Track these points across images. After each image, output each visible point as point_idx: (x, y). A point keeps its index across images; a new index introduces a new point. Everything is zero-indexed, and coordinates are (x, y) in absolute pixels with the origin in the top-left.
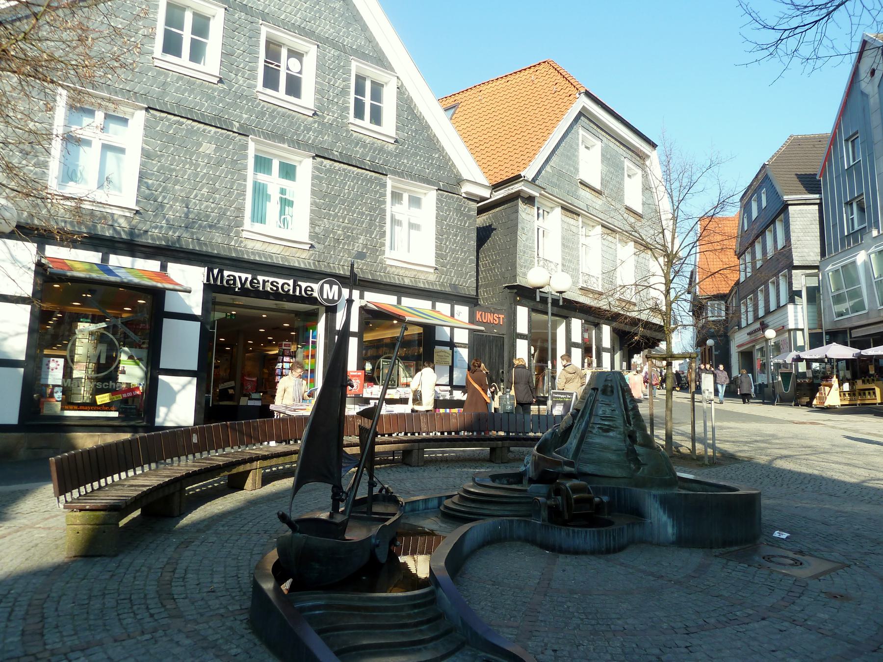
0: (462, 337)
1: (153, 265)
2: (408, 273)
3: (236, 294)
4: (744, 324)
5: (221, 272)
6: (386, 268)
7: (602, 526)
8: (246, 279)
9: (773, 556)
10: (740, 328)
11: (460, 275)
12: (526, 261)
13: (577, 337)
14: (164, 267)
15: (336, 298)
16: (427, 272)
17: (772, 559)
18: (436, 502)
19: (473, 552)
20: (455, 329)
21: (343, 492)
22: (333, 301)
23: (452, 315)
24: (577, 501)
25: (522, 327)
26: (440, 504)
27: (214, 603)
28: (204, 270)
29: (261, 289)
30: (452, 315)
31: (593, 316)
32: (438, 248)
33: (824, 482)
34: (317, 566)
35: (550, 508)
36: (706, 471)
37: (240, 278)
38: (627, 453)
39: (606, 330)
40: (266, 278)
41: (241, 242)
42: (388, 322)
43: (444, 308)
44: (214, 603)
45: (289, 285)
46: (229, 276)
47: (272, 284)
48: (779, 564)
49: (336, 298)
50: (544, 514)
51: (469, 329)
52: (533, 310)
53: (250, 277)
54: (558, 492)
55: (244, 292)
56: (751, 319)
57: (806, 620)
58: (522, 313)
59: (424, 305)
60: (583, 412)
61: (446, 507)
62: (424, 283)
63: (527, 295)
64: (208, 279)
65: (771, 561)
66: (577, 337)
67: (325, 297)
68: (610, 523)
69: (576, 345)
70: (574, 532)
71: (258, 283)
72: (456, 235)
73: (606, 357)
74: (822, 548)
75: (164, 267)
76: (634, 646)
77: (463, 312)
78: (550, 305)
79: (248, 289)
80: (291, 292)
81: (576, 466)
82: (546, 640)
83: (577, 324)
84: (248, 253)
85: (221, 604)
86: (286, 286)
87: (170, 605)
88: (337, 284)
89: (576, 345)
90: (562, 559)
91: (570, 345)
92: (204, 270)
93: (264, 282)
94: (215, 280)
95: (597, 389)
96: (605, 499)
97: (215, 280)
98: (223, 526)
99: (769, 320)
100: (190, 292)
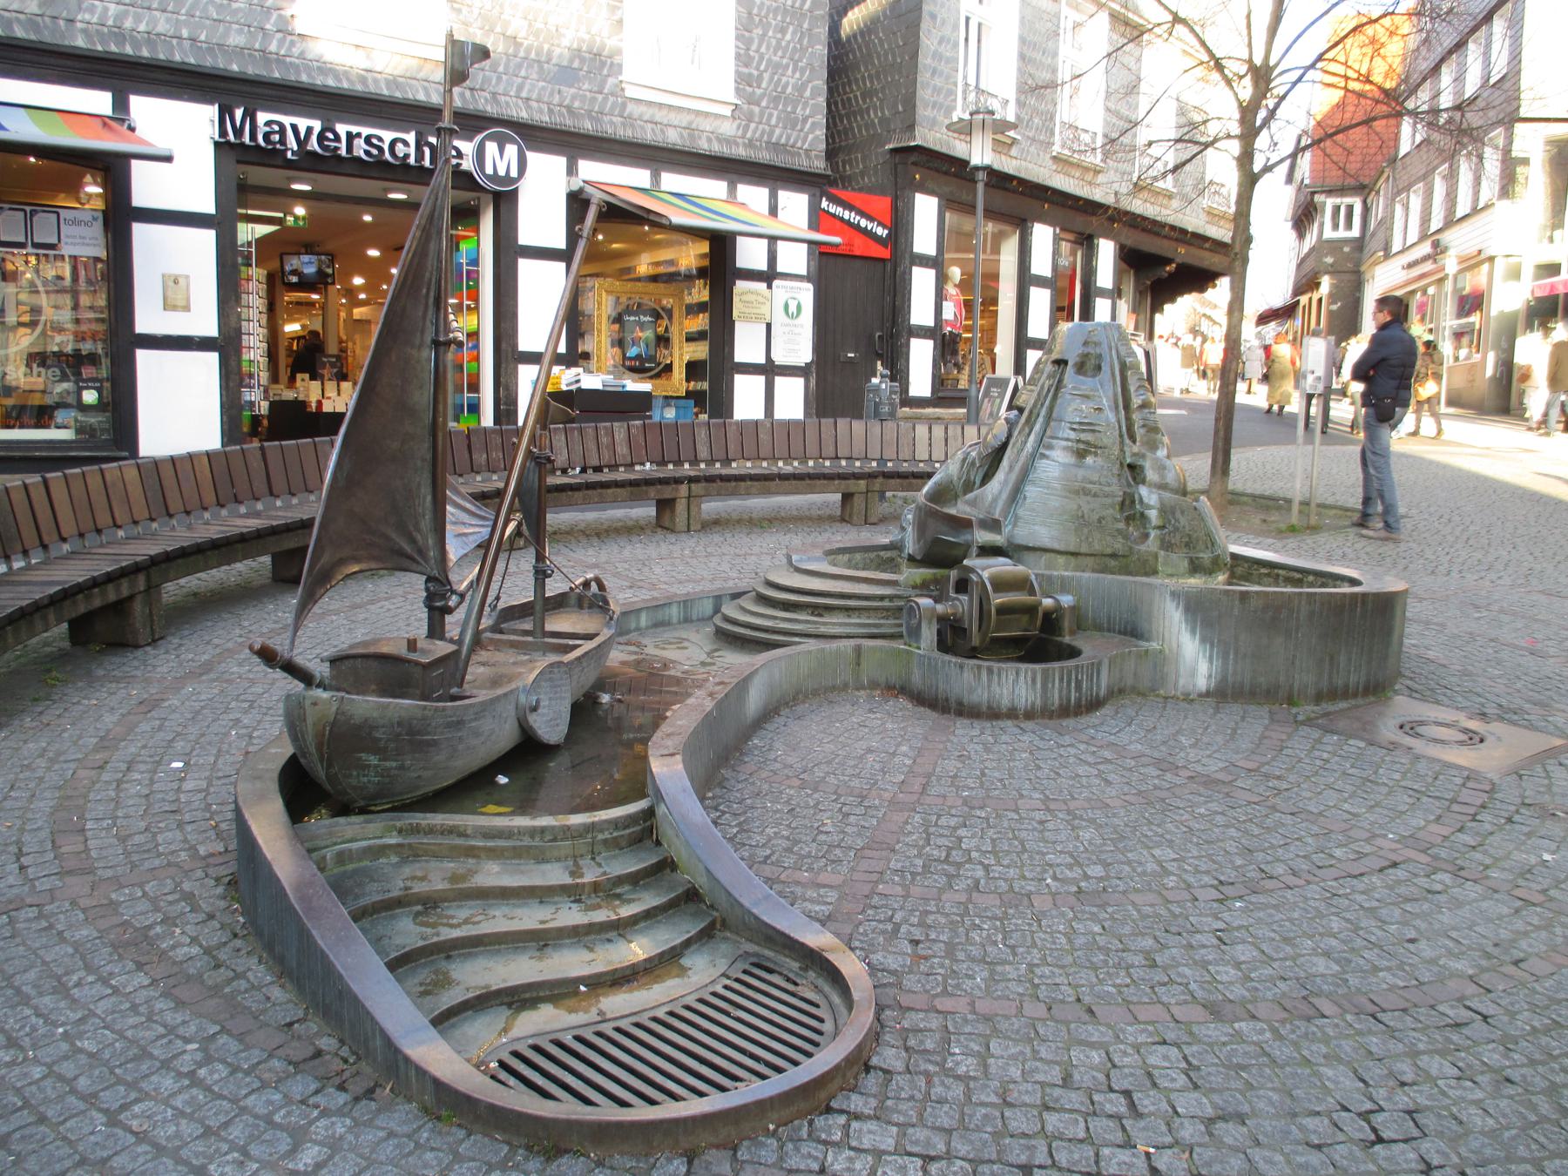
0: (794, 259)
1: (98, 101)
2: (674, 118)
3: (290, 165)
4: (1396, 247)
5: (250, 114)
6: (624, 105)
7: (1059, 658)
8: (309, 130)
9: (1422, 723)
10: (1387, 256)
11: (790, 122)
12: (938, 91)
13: (1041, 264)
14: (121, 105)
15: (514, 173)
16: (717, 116)
17: (1420, 730)
18: (708, 607)
19: (768, 714)
20: (779, 243)
21: (453, 592)
22: (508, 179)
23: (773, 211)
24: (1003, 610)
25: (924, 239)
26: (717, 610)
27: (169, 838)
28: (212, 111)
29: (343, 152)
30: (773, 211)
31: (1081, 218)
32: (743, 59)
33: (167, 473)
34: (373, 760)
35: (942, 619)
36: (1292, 542)
37: (295, 128)
38: (1122, 504)
39: (1106, 251)
40: (355, 129)
41: (293, 43)
42: (636, 229)
43: (754, 196)
44: (169, 838)
45: (406, 143)
46: (268, 123)
47: (368, 140)
48: (1436, 741)
49: (514, 173)
50: (929, 634)
51: (810, 242)
52: (949, 203)
53: (317, 125)
54: (962, 586)
55: (309, 162)
56: (1413, 236)
57: (1487, 867)
58: (926, 208)
59: (711, 188)
60: (1031, 412)
61: (727, 619)
62: (709, 140)
63: (948, 173)
64: (223, 133)
65: (1419, 735)
66: (1041, 264)
67: (489, 170)
68: (1074, 653)
69: (1041, 282)
70: (990, 671)
71: (337, 138)
72: (783, 31)
73: (1102, 308)
74: (1527, 706)
75: (121, 105)
76: (1097, 929)
77: (795, 204)
78: (980, 187)
79: (314, 153)
80: (412, 161)
81: (1007, 530)
82: (898, 917)
83: (1042, 235)
84: (308, 69)
85: (185, 841)
86: (400, 146)
87: (70, 846)
88: (513, 141)
89: (1041, 282)
90: (964, 732)
91: (1025, 280)
92: (212, 111)
93: (351, 137)
94: (239, 132)
95: (1066, 362)
96: (1066, 600)
97: (239, 132)
98: (240, 665)
99: (1451, 237)
100: (168, 159)
